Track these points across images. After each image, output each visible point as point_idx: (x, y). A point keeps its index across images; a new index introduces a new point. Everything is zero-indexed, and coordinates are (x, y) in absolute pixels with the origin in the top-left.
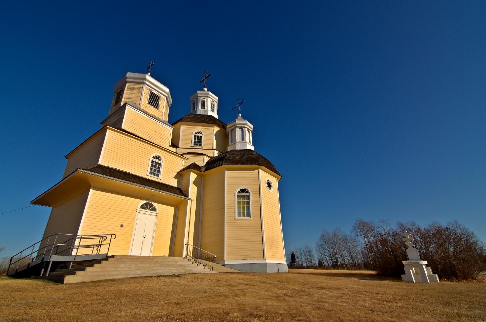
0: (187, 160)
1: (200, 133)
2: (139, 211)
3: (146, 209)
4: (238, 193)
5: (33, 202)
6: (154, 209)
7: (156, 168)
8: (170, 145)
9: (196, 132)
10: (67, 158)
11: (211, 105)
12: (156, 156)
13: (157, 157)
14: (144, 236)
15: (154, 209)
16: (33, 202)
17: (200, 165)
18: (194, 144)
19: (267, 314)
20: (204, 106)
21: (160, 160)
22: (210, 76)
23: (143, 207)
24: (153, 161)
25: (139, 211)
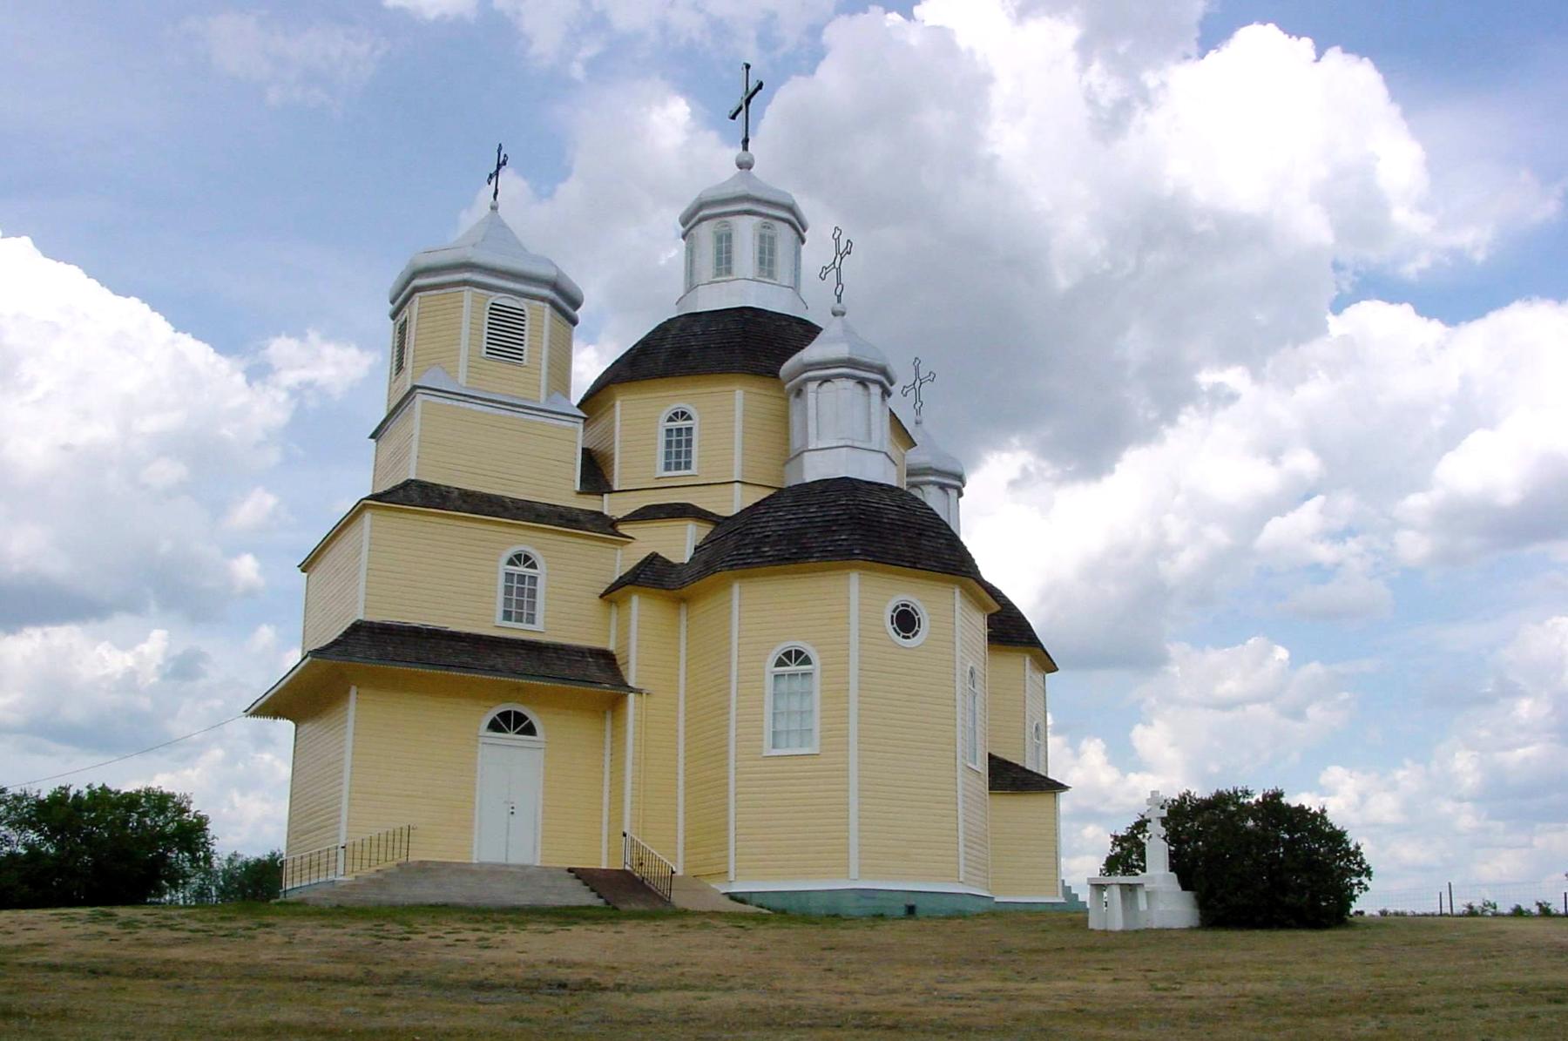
0: (630, 546)
1: (684, 415)
2: (487, 740)
3: (504, 731)
4: (777, 665)
5: (251, 710)
6: (530, 730)
7: (520, 595)
8: (578, 488)
9: (671, 414)
10: (303, 571)
11: (757, 243)
12: (518, 556)
13: (522, 559)
14: (511, 810)
15: (530, 730)
16: (249, 712)
17: (675, 560)
18: (668, 467)
19: (331, 1033)
20: (729, 260)
21: (533, 566)
22: (245, 709)
23: (494, 726)
24: (509, 576)
25: (487, 740)
